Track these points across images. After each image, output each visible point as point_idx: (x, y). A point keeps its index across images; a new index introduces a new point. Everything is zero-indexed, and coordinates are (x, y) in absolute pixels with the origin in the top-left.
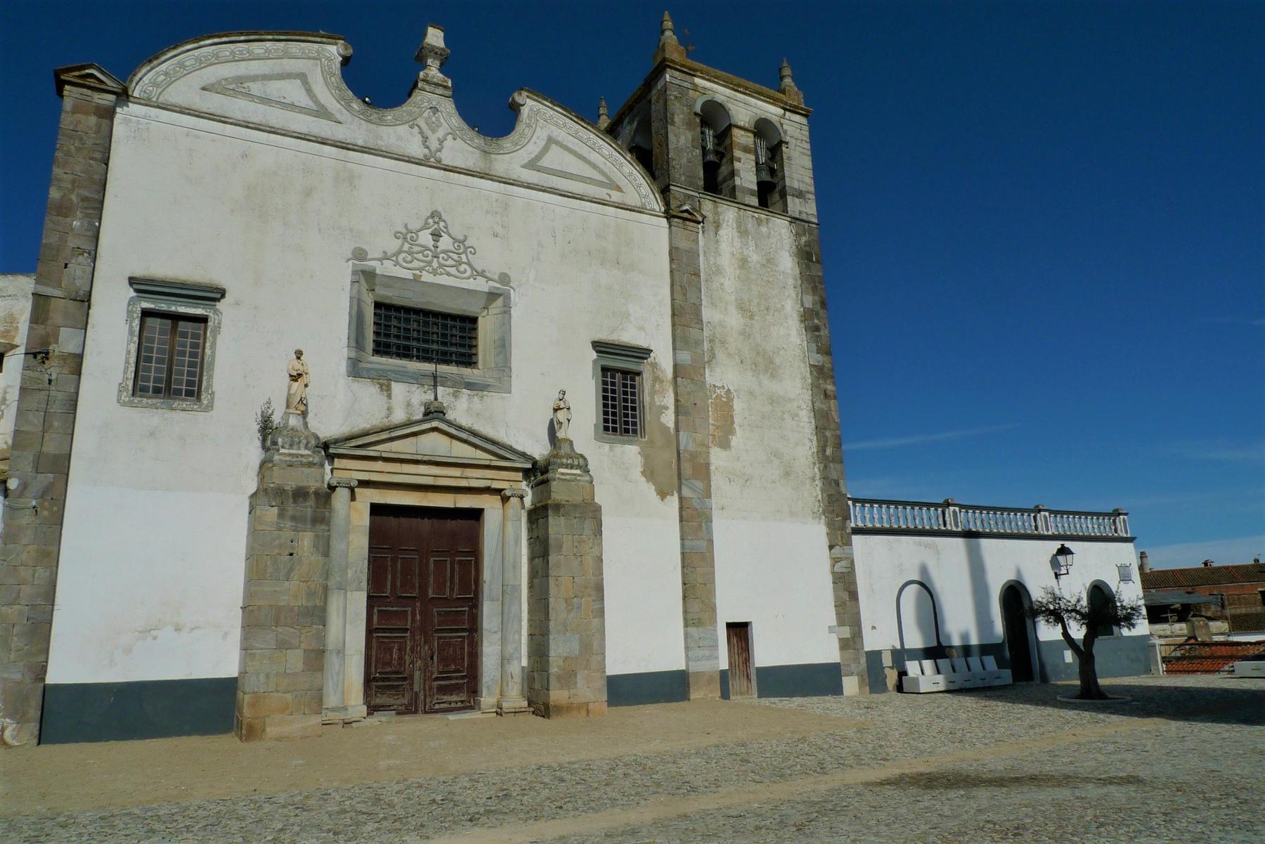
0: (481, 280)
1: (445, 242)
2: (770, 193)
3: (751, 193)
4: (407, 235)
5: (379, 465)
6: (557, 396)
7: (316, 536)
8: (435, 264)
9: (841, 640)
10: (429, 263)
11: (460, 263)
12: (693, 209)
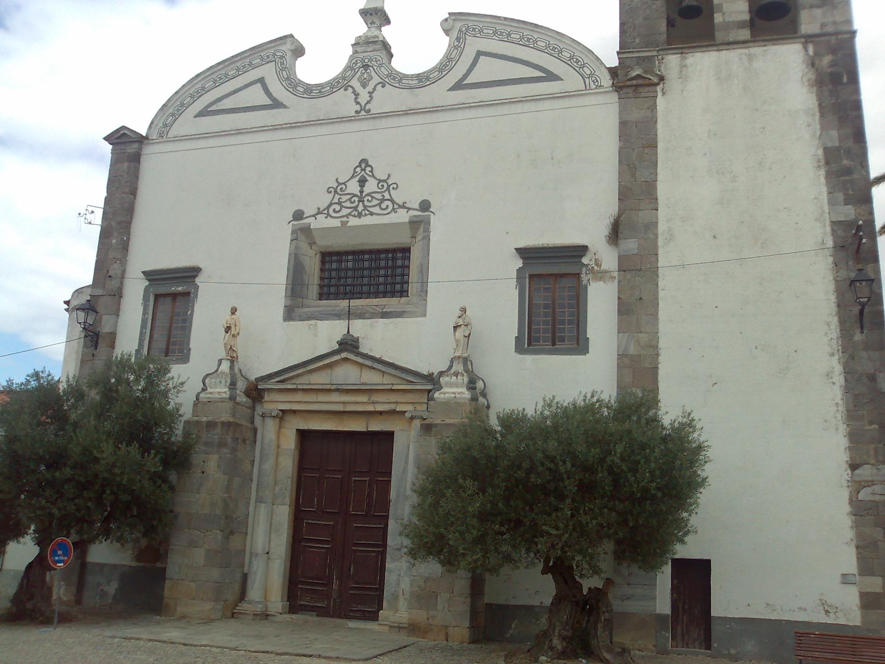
0: (402, 212)
1: (371, 186)
2: (650, 59)
3: (741, 25)
4: (338, 189)
5: (299, 397)
6: (459, 313)
7: (220, 458)
8: (361, 208)
9: (863, 595)
10: (355, 208)
11: (383, 200)
12: (645, 72)
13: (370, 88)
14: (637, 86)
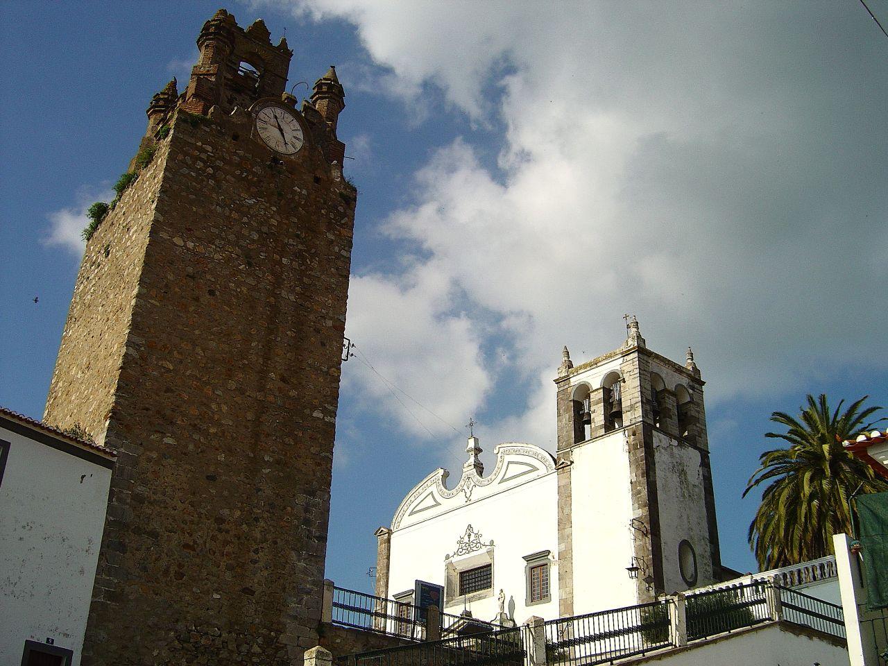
1: (472, 538)
13: (470, 489)
14: (563, 467)
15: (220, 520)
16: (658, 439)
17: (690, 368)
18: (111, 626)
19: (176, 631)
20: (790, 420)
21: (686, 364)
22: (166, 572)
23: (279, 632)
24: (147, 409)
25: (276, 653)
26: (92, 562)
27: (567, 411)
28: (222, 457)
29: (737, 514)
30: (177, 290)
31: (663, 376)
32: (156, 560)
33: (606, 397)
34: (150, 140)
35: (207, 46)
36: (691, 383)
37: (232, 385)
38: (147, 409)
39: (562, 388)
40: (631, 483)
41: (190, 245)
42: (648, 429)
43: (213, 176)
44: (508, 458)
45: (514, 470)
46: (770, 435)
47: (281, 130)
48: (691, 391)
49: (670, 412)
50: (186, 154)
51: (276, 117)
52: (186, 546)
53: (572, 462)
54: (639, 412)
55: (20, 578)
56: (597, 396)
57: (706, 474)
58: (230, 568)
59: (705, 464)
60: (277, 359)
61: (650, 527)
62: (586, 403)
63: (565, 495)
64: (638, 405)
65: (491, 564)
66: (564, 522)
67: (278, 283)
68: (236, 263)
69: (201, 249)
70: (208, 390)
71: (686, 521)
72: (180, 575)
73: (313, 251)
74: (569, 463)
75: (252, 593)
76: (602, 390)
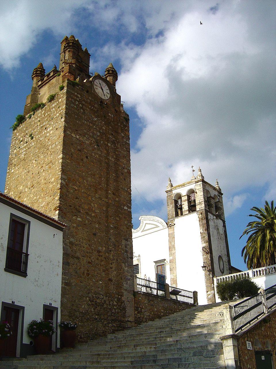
15: (99, 252)
16: (210, 216)
17: (218, 188)
18: (67, 296)
19: (89, 298)
20: (258, 210)
21: (216, 186)
22: (83, 273)
23: (122, 296)
24: (71, 206)
25: (121, 304)
26: (60, 270)
27: (171, 204)
28: (97, 226)
29: (238, 244)
30: (75, 156)
31: (210, 191)
32: (80, 268)
33: (188, 199)
34: (35, 88)
35: (69, 51)
36: (218, 194)
37: (97, 196)
38: (71, 206)
39: (169, 195)
40: (201, 233)
41: (78, 137)
42: (207, 212)
43: (82, 108)
44: (145, 222)
45: (148, 227)
46: (250, 215)
47: (102, 89)
48: (219, 197)
49: (214, 206)
50: (72, 98)
51: (100, 84)
52: (89, 263)
53: (175, 224)
54: (203, 205)
55: (39, 279)
56: (185, 198)
57: (225, 230)
58: (104, 271)
59: (224, 226)
60: (111, 185)
61: (209, 250)
62: (179, 201)
63: (172, 237)
64: (202, 202)
65: (138, 265)
66: (172, 248)
67: (108, 154)
68: (94, 145)
69: (81, 139)
70: (90, 198)
71: (220, 248)
72: (88, 274)
73: (118, 141)
74: (173, 225)
75: (112, 281)
76: (187, 196)
